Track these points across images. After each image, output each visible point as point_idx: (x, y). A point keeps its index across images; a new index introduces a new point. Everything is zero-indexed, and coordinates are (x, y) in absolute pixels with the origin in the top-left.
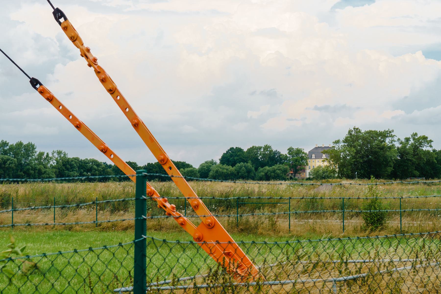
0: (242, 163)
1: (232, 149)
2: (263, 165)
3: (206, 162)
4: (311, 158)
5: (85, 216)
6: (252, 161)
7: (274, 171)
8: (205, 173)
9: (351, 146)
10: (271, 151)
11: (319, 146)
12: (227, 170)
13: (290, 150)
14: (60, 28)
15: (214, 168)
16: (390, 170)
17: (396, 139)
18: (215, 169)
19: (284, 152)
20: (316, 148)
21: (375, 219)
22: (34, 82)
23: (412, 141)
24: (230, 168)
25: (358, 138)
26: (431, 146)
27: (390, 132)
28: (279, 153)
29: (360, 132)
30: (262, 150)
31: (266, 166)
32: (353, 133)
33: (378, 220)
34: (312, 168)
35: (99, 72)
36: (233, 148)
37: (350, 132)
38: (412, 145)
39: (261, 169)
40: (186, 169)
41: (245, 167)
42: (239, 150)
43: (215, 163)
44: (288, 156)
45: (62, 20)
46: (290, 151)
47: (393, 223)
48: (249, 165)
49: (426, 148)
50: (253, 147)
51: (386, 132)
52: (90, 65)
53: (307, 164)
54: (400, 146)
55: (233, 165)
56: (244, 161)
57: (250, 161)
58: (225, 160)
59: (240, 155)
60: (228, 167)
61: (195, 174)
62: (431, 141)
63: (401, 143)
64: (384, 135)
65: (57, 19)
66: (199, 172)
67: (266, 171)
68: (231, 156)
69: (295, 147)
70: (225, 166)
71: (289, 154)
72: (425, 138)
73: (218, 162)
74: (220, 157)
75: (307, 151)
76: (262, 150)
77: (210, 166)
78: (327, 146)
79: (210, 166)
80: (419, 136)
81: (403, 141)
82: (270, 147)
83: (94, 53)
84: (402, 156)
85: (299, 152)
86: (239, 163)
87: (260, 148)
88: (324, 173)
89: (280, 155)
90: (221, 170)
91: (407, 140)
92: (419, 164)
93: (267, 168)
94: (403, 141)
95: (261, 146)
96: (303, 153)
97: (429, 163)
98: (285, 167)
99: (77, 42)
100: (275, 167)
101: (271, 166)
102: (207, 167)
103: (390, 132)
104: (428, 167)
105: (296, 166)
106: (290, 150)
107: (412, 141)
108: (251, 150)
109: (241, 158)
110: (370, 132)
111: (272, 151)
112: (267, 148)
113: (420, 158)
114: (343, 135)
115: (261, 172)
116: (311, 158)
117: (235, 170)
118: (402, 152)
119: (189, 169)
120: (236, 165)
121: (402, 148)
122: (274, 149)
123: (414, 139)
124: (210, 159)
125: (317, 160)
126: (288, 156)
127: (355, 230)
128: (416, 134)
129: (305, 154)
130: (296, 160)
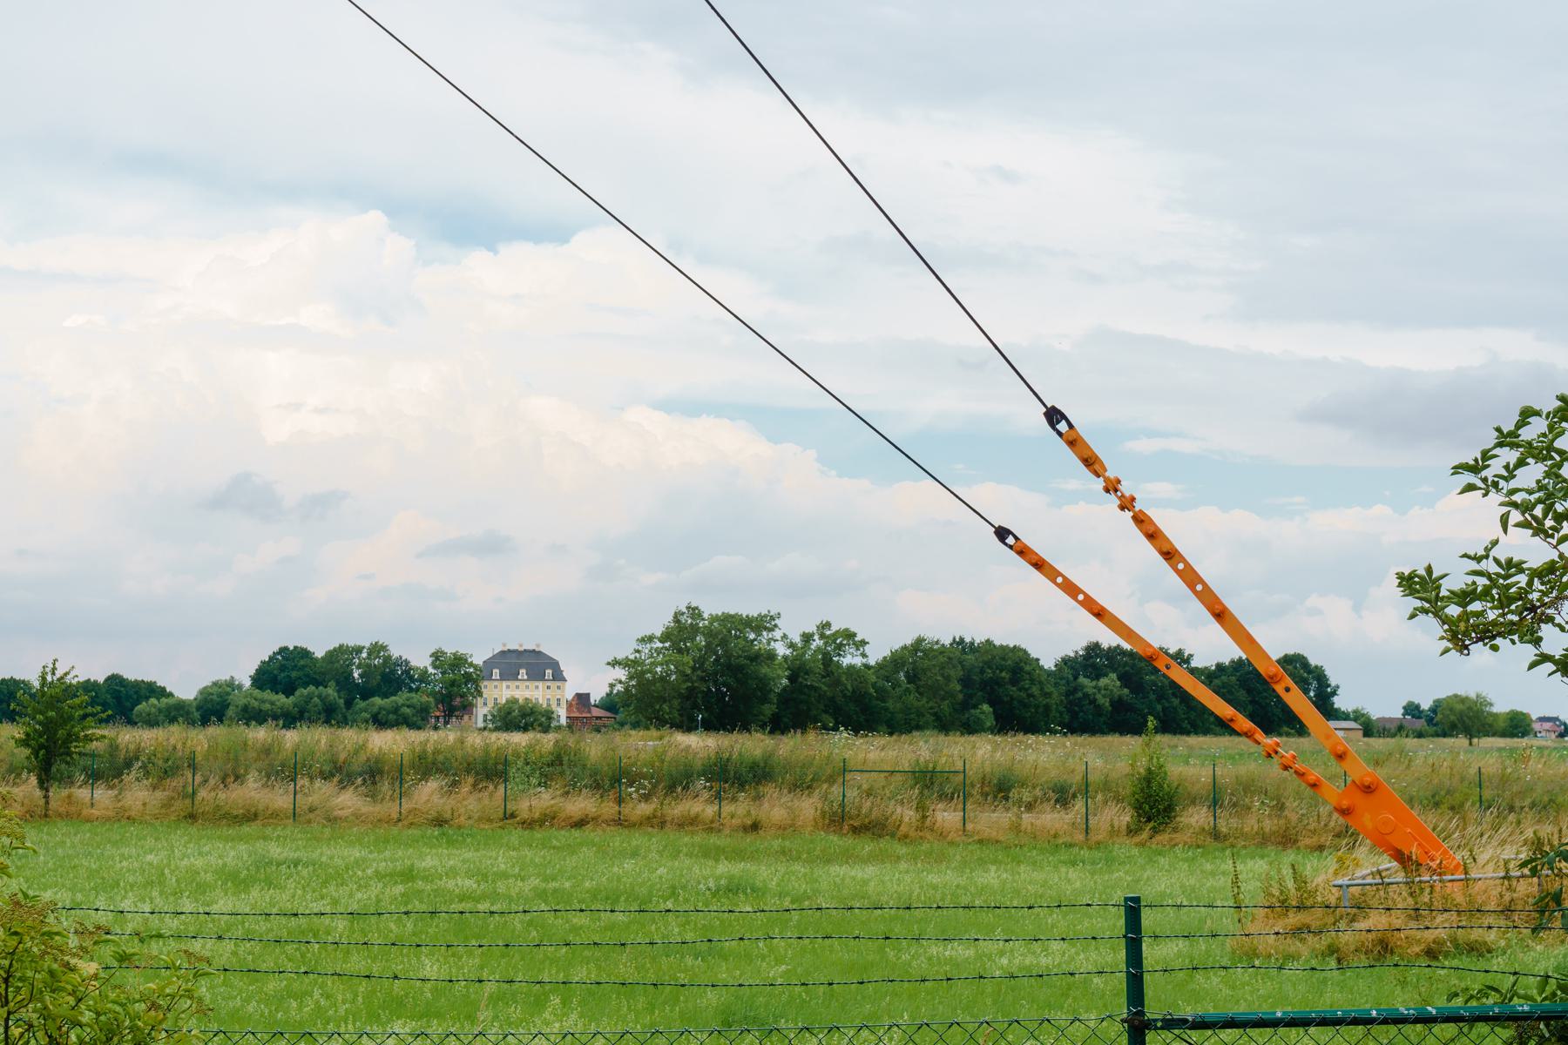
0: (312, 688)
1: (283, 650)
2: (366, 694)
3: (215, 684)
4: (490, 678)
5: (429, 793)
6: (338, 683)
7: (396, 710)
8: (214, 707)
9: (680, 651)
10: (388, 659)
11: (512, 647)
12: (272, 703)
13: (437, 656)
14: (1061, 445)
15: (238, 700)
16: (769, 709)
17: (777, 634)
18: (242, 702)
19: (420, 660)
20: (503, 652)
21: (1155, 807)
22: (1002, 533)
23: (817, 642)
24: (281, 699)
25: (695, 630)
26: (864, 655)
27: (772, 618)
28: (407, 662)
29: (700, 615)
30: (364, 655)
31: (373, 695)
32: (683, 619)
33: (1165, 810)
34: (491, 704)
35: (1140, 520)
36: (286, 648)
37: (676, 619)
38: (818, 649)
39: (362, 704)
40: (164, 700)
41: (319, 696)
42: (304, 653)
43: (240, 687)
44: (431, 670)
45: (1063, 426)
46: (437, 658)
47: (1195, 817)
48: (331, 692)
49: (850, 659)
50: (341, 646)
51: (761, 618)
52: (1122, 508)
53: (480, 694)
54: (788, 652)
55: (289, 690)
56: (317, 684)
57: (332, 683)
58: (267, 677)
59: (304, 666)
60: (273, 697)
61: (188, 713)
62: (864, 643)
63: (792, 645)
64: (762, 624)
65: (1053, 425)
66: (198, 708)
67: (375, 709)
68: (282, 668)
69: (449, 650)
70: (268, 695)
71: (435, 667)
72: (850, 635)
73: (247, 683)
74: (252, 672)
75: (478, 660)
76: (364, 655)
77: (228, 694)
78: (531, 647)
79: (228, 694)
80: (834, 628)
81: (797, 640)
82: (384, 648)
83: (1126, 488)
84: (792, 679)
85: (459, 661)
86: (305, 685)
87: (359, 650)
88: (524, 715)
89: (408, 671)
90: (256, 704)
91: (807, 638)
92: (832, 699)
93: (377, 701)
94: (797, 640)
95: (359, 643)
96: (471, 665)
97: (859, 697)
98: (425, 699)
99: (1096, 467)
100: (400, 698)
101: (385, 696)
102: (220, 695)
103: (772, 618)
104: (852, 707)
105: (450, 696)
106: (437, 656)
107: (817, 642)
108: (333, 655)
109: (308, 676)
110: (727, 619)
111: (390, 657)
112: (377, 649)
113: (837, 682)
114: (659, 623)
115: (361, 710)
116: (490, 678)
117: (295, 705)
118: (797, 669)
119: (170, 701)
120: (297, 693)
121: (795, 659)
122: (395, 652)
123: (822, 636)
124: (225, 677)
125: (505, 684)
126: (431, 670)
127: (1113, 832)
128: (828, 625)
129: (475, 667)
130: (453, 683)
